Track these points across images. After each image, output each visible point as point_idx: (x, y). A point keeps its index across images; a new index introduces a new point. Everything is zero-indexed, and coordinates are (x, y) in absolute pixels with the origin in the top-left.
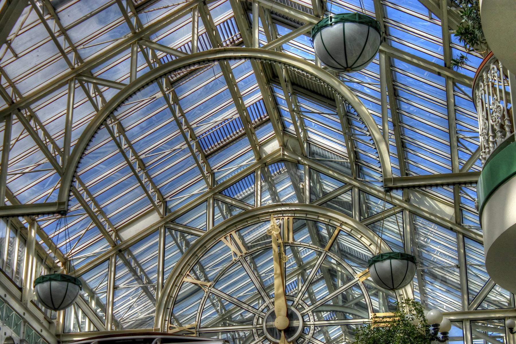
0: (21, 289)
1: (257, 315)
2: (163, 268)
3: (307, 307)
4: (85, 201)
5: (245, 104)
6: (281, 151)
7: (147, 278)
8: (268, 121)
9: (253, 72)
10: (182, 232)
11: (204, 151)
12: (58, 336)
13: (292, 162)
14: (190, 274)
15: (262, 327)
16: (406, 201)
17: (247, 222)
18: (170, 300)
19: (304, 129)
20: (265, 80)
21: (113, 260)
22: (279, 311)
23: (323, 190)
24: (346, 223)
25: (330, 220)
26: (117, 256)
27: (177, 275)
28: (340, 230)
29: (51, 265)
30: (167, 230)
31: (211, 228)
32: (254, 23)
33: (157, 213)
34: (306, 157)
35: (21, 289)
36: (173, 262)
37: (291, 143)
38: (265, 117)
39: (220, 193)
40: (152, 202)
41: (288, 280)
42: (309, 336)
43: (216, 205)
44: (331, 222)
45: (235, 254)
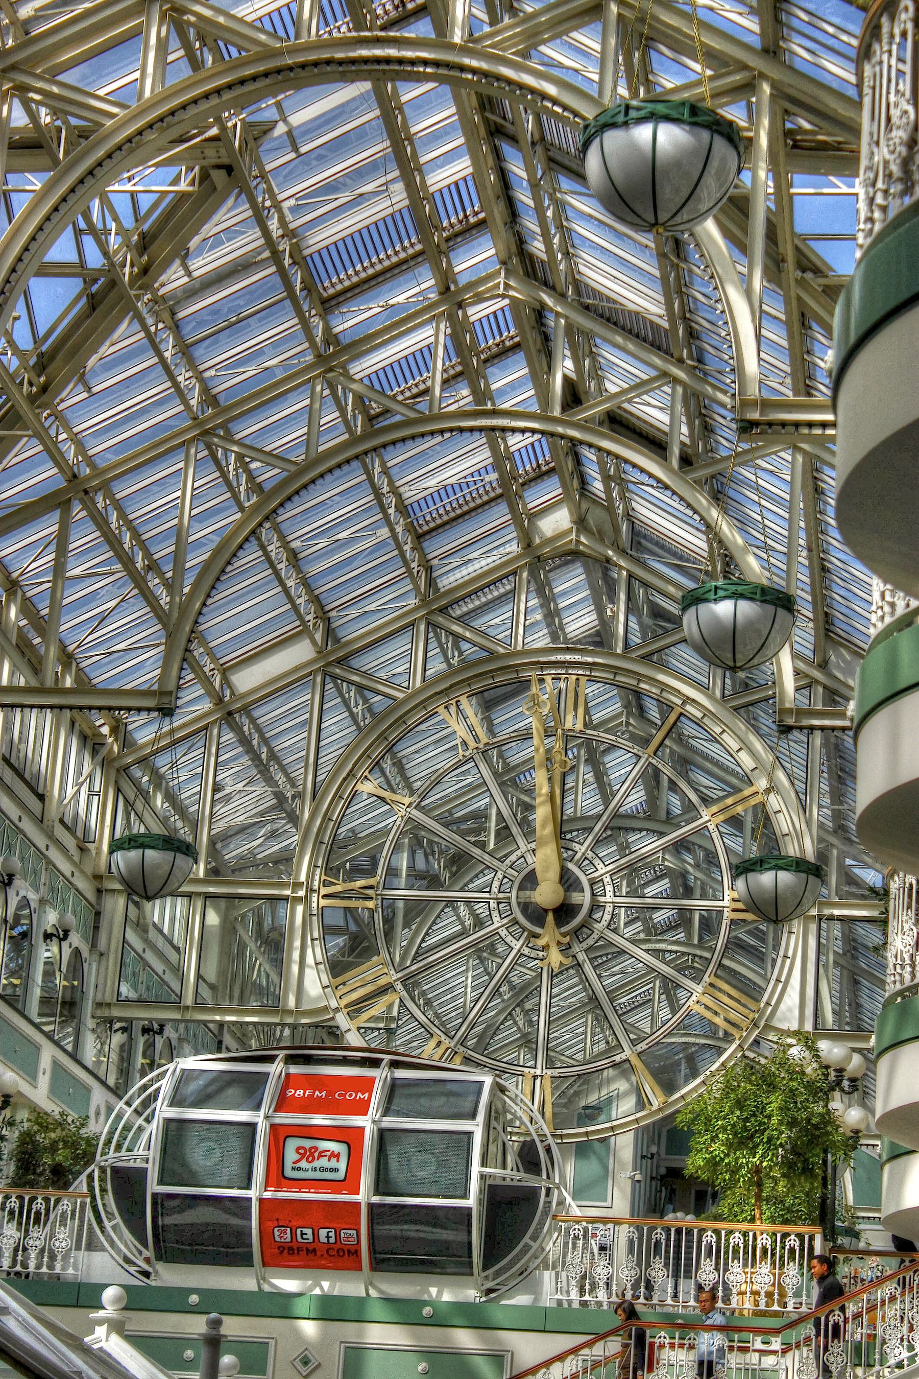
0: (41, 797)
1: (500, 872)
2: (317, 758)
3: (602, 865)
4: (42, 424)
5: (429, 183)
6: (574, 533)
7: (148, 555)
8: (552, 470)
9: (532, 392)
10: (360, 688)
11: (319, 285)
12: (98, 877)
13: (596, 560)
15: (509, 898)
16: (820, 666)
18: (327, 824)
19: (562, 226)
20: (483, 132)
21: (215, 731)
22: (546, 869)
23: (577, 277)
24: (694, 700)
25: (662, 690)
26: (225, 726)
27: (344, 775)
28: (681, 714)
29: (89, 732)
30: (328, 679)
31: (418, 683)
32: (555, 337)
33: (308, 641)
34: (624, 551)
35: (41, 797)
37: (595, 517)
38: (547, 463)
39: (443, 610)
40: (185, 401)
43: (431, 635)
44: (665, 694)
45: (464, 743)
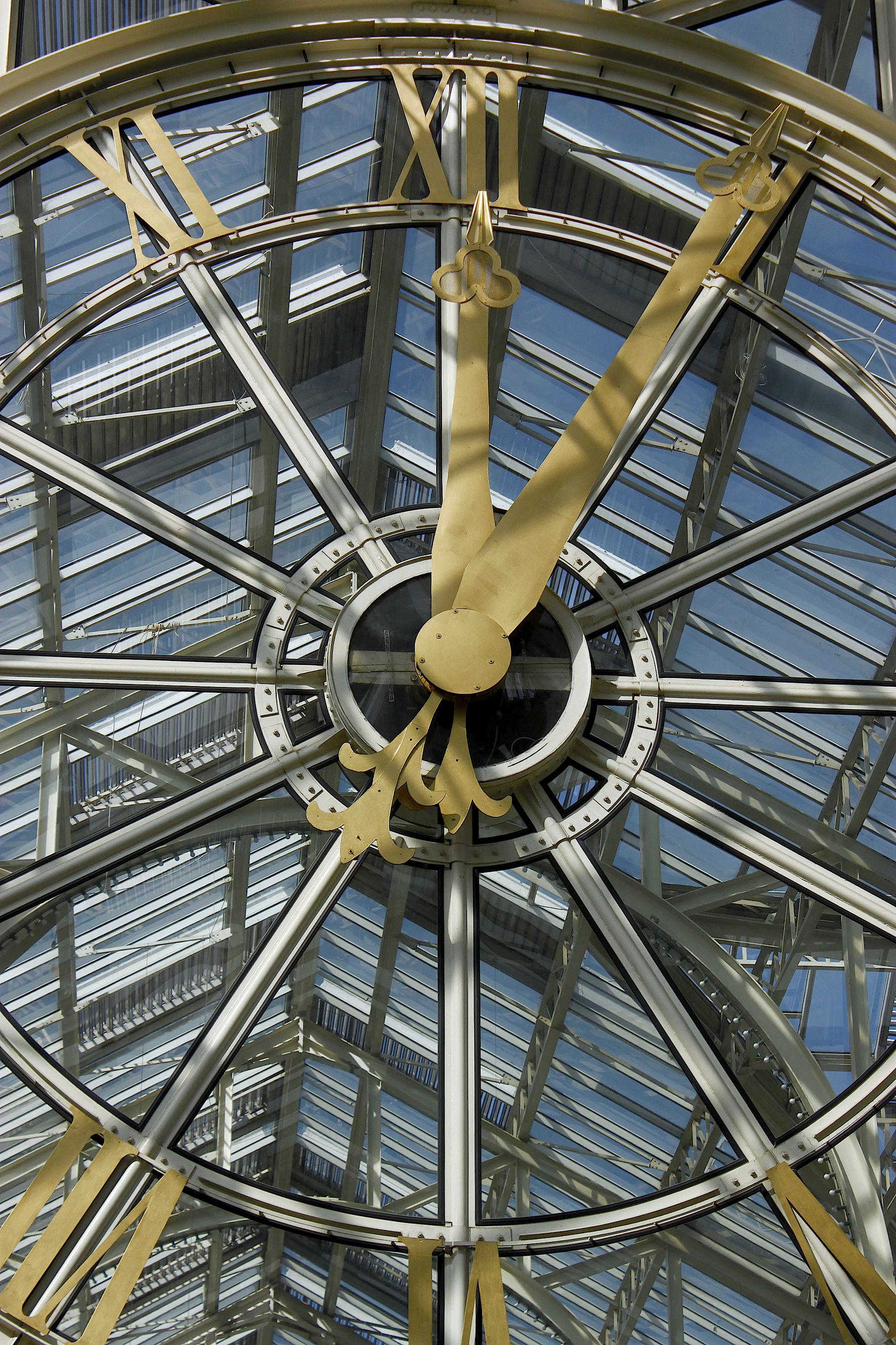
24: (845, 139)
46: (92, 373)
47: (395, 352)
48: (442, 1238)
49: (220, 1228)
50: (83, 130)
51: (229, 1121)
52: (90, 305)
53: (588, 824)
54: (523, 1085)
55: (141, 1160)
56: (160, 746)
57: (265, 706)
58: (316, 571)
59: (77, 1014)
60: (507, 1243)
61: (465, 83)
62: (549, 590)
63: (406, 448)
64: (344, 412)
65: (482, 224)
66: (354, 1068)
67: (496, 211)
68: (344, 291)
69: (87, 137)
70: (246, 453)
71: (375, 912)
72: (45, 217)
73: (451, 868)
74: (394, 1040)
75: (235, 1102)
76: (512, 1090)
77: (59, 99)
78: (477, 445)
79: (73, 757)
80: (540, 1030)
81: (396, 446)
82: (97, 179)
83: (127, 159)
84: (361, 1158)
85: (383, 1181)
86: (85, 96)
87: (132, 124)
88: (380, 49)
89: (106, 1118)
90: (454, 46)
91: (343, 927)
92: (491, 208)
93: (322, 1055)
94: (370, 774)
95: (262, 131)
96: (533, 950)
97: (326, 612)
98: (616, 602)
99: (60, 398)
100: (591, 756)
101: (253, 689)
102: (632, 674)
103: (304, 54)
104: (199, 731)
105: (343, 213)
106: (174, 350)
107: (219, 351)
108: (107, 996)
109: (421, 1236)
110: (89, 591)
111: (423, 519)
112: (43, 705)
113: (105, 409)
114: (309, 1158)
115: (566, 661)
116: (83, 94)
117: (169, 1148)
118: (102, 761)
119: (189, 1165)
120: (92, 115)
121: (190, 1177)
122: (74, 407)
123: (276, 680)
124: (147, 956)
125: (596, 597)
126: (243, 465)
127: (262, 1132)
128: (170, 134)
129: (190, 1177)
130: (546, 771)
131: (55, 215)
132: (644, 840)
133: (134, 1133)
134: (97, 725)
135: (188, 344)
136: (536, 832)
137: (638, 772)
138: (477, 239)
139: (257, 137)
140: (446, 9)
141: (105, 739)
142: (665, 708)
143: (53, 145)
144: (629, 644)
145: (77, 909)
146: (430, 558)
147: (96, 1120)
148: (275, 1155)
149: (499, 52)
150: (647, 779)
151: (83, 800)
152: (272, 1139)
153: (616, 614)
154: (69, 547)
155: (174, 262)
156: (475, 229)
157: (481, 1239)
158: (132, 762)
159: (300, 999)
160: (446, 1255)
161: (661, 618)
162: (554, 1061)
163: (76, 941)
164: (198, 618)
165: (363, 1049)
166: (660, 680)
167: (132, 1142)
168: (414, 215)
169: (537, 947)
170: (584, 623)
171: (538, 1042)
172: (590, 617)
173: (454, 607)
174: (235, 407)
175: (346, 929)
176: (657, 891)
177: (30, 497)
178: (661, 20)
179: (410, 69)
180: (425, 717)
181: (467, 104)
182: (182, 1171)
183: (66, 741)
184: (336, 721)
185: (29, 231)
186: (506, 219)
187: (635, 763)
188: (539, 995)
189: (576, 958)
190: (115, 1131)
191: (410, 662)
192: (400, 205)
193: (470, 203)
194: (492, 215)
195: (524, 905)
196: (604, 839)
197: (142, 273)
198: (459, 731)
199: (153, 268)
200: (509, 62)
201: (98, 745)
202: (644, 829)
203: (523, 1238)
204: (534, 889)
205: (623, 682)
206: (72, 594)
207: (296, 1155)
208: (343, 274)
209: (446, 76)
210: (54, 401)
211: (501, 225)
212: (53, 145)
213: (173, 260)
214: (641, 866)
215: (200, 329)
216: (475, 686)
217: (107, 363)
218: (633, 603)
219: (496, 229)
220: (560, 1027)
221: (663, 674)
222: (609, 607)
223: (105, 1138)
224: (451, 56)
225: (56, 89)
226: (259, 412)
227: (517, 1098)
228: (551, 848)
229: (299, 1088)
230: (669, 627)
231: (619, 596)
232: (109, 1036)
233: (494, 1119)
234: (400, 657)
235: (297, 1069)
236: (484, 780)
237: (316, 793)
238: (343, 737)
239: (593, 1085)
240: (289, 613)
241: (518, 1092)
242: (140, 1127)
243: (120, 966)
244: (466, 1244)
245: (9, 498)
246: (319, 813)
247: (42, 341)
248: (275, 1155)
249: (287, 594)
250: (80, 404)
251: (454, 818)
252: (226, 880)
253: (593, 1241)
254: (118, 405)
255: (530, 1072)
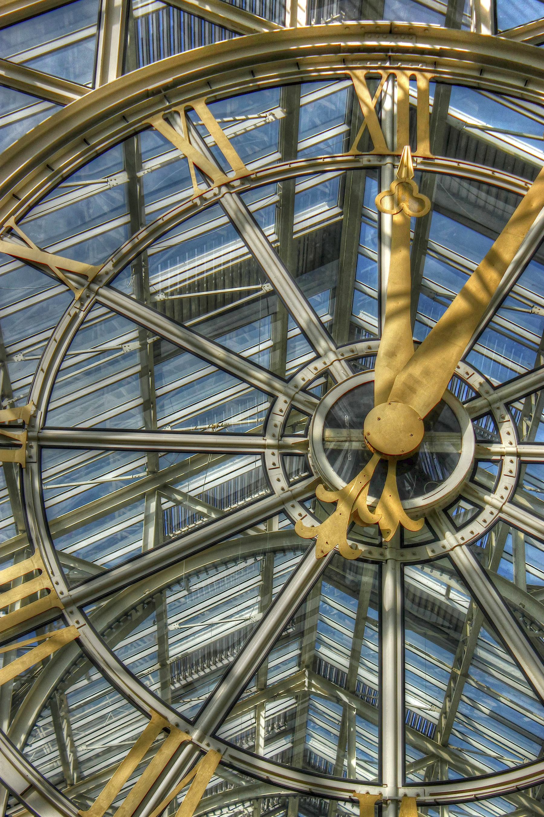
14: (18, 230)
17: (253, 73)
36: (61, 383)
41: (68, 383)
42: (497, 495)
46: (174, 270)
47: (360, 256)
48: (381, 794)
49: (257, 799)
50: (163, 113)
51: (262, 732)
52: (166, 219)
53: (472, 536)
54: (444, 712)
55: (193, 743)
56: (218, 498)
57: (271, 463)
58: (303, 379)
59: (169, 666)
60: (422, 798)
61: (396, 81)
62: (449, 391)
63: (367, 315)
64: (328, 293)
65: (407, 166)
66: (339, 700)
67: (415, 159)
68: (328, 218)
69: (165, 117)
70: (268, 319)
71: (351, 604)
72: (143, 172)
73: (386, 563)
74: (364, 684)
75: (267, 722)
76: (436, 714)
77: (147, 94)
78: (402, 302)
79: (165, 507)
80: (453, 677)
81: (361, 314)
82: (177, 149)
83: (189, 130)
84: (344, 756)
85: (357, 771)
86: (163, 93)
87: (192, 109)
88: (344, 61)
89: (172, 718)
90: (390, 58)
91: (333, 613)
92: (413, 157)
93: (319, 692)
94: (335, 504)
95: (275, 118)
96: (449, 628)
97: (310, 405)
98: (490, 398)
99: (155, 284)
100: (474, 493)
101: (264, 452)
102: (500, 442)
103: (297, 65)
104: (242, 490)
105: (321, 161)
106: (224, 255)
107: (250, 256)
108: (187, 654)
109: (368, 793)
110: (173, 404)
111: (369, 348)
112: (145, 473)
113: (181, 291)
114: (313, 757)
115: (458, 434)
116: (162, 91)
117: (210, 736)
118: (183, 508)
119: (223, 747)
120: (168, 104)
121: (224, 754)
122: (163, 290)
123: (279, 447)
124: (211, 630)
125: (478, 395)
126: (267, 327)
127: (284, 741)
128: (219, 120)
129: (224, 754)
130: (446, 503)
131: (149, 170)
132: (515, 557)
133: (189, 727)
134: (180, 487)
135: (232, 251)
136: (440, 540)
137: (504, 504)
138: (403, 175)
139: (272, 122)
140: (385, 36)
141: (184, 495)
142: (521, 464)
143: (143, 122)
144: (498, 424)
145: (169, 600)
146: (374, 371)
147: (166, 718)
148: (292, 757)
149: (417, 62)
150: (509, 508)
151: (172, 533)
152: (290, 745)
153: (490, 405)
154: (161, 376)
155: (217, 192)
156: (403, 169)
157: (405, 795)
158: (199, 508)
159: (306, 657)
160: (384, 805)
161: (525, 418)
162: (462, 696)
163: (168, 620)
164: (242, 420)
165: (345, 689)
166: (518, 447)
167: (188, 732)
168: (365, 161)
169: (451, 626)
170: (470, 411)
171: (452, 685)
172: (474, 407)
173: (389, 401)
174: (260, 289)
175: (334, 615)
176: (523, 587)
177: (136, 345)
178: (518, 40)
179: (362, 73)
180: (370, 468)
181: (398, 94)
182: (219, 751)
183: (160, 496)
184: (315, 472)
185: (134, 181)
186: (422, 163)
187: (502, 498)
188: (453, 655)
189: (476, 632)
190: (177, 725)
191: (361, 435)
192: (356, 156)
193: (400, 154)
194: (413, 160)
195: (443, 599)
196: (491, 557)
197: (197, 199)
198: (392, 477)
199: (204, 196)
200: (424, 68)
201: (179, 498)
202: (515, 550)
203: (431, 795)
204: (449, 589)
205: (495, 448)
206: (163, 406)
207: (305, 756)
208: (327, 208)
209: (385, 76)
210: (151, 286)
211: (419, 167)
212: (143, 122)
213: (216, 190)
214: (514, 573)
215: (239, 242)
216: (401, 450)
217: (183, 264)
218: (501, 399)
219: (416, 170)
220: (466, 675)
221: (520, 442)
222: (485, 401)
223: (171, 729)
224: (388, 64)
225: (146, 89)
226: (274, 292)
227: (440, 720)
228: (449, 551)
229: (306, 714)
230: (530, 423)
231: (492, 394)
232: (190, 679)
233: (426, 733)
234: (355, 433)
235: (306, 701)
236: (407, 508)
237: (303, 516)
238: (319, 481)
239: (487, 712)
240: (286, 405)
241: (441, 716)
242: (193, 723)
243: (196, 636)
244: (396, 798)
245: (123, 345)
246: (302, 527)
247: (136, 241)
248: (292, 757)
249: (286, 394)
250: (166, 288)
251: (388, 532)
252: (260, 583)
253: (476, 798)
254: (191, 288)
255: (448, 704)
